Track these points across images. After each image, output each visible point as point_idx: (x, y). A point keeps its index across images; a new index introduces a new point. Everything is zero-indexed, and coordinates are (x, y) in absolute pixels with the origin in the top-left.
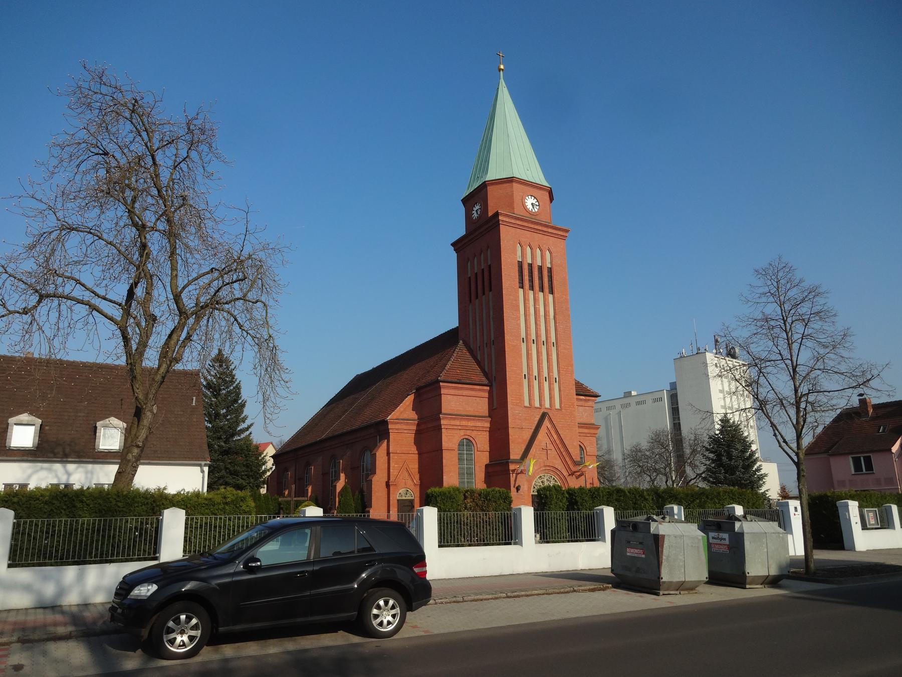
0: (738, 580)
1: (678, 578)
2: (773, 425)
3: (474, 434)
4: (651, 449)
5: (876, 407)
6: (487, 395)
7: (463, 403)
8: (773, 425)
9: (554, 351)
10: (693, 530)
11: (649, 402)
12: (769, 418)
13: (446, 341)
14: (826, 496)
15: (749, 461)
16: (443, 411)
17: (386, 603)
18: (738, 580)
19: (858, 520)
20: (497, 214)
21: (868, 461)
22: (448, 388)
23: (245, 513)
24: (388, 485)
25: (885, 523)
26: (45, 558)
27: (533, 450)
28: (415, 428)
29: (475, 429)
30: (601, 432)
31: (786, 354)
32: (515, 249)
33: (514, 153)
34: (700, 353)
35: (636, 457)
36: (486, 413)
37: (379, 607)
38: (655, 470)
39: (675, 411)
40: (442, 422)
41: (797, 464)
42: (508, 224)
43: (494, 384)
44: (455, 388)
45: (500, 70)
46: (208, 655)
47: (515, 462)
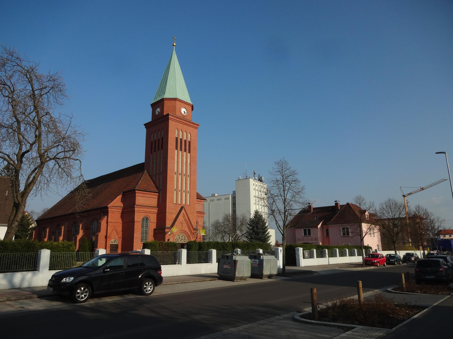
0: (260, 276)
1: (241, 275)
2: (276, 221)
3: (149, 215)
4: (224, 223)
5: (314, 209)
6: (157, 197)
7: (145, 201)
8: (276, 221)
9: (189, 178)
10: (246, 258)
11: (223, 199)
12: (275, 217)
13: (137, 169)
14: (292, 246)
15: (264, 229)
16: (136, 204)
17: (149, 283)
18: (260, 276)
19: (302, 255)
20: (168, 115)
21: (309, 231)
23: (72, 251)
24: (106, 237)
25: (311, 256)
27: (176, 223)
28: (121, 211)
29: (150, 212)
30: (206, 216)
31: (283, 194)
32: (175, 131)
33: (177, 87)
34: (247, 178)
35: (216, 226)
36: (156, 205)
37: (146, 285)
38: (225, 232)
39: (234, 204)
40: (136, 209)
41: (283, 235)
42: (172, 120)
43: (161, 192)
44: (142, 193)
45: (174, 45)
46: (92, 302)
47: (168, 228)
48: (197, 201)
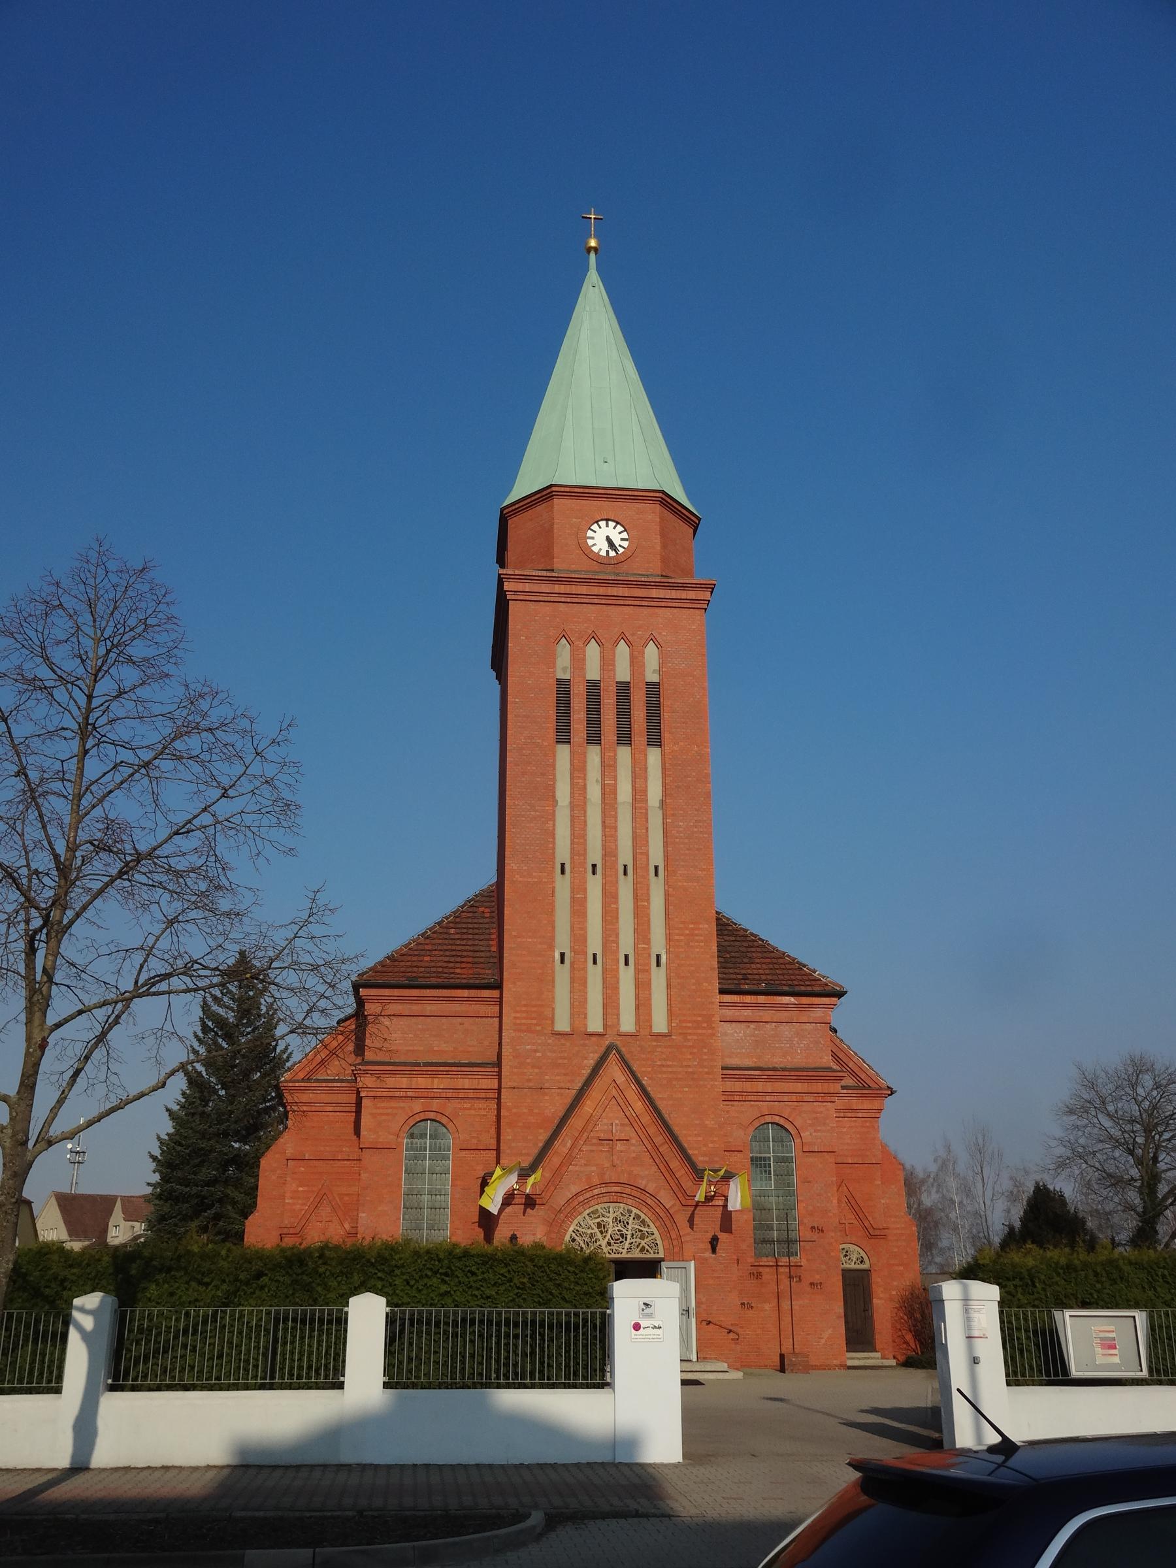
22: (378, 998)
26: (21, 1381)
45: (589, 250)
48: (722, 1005)
